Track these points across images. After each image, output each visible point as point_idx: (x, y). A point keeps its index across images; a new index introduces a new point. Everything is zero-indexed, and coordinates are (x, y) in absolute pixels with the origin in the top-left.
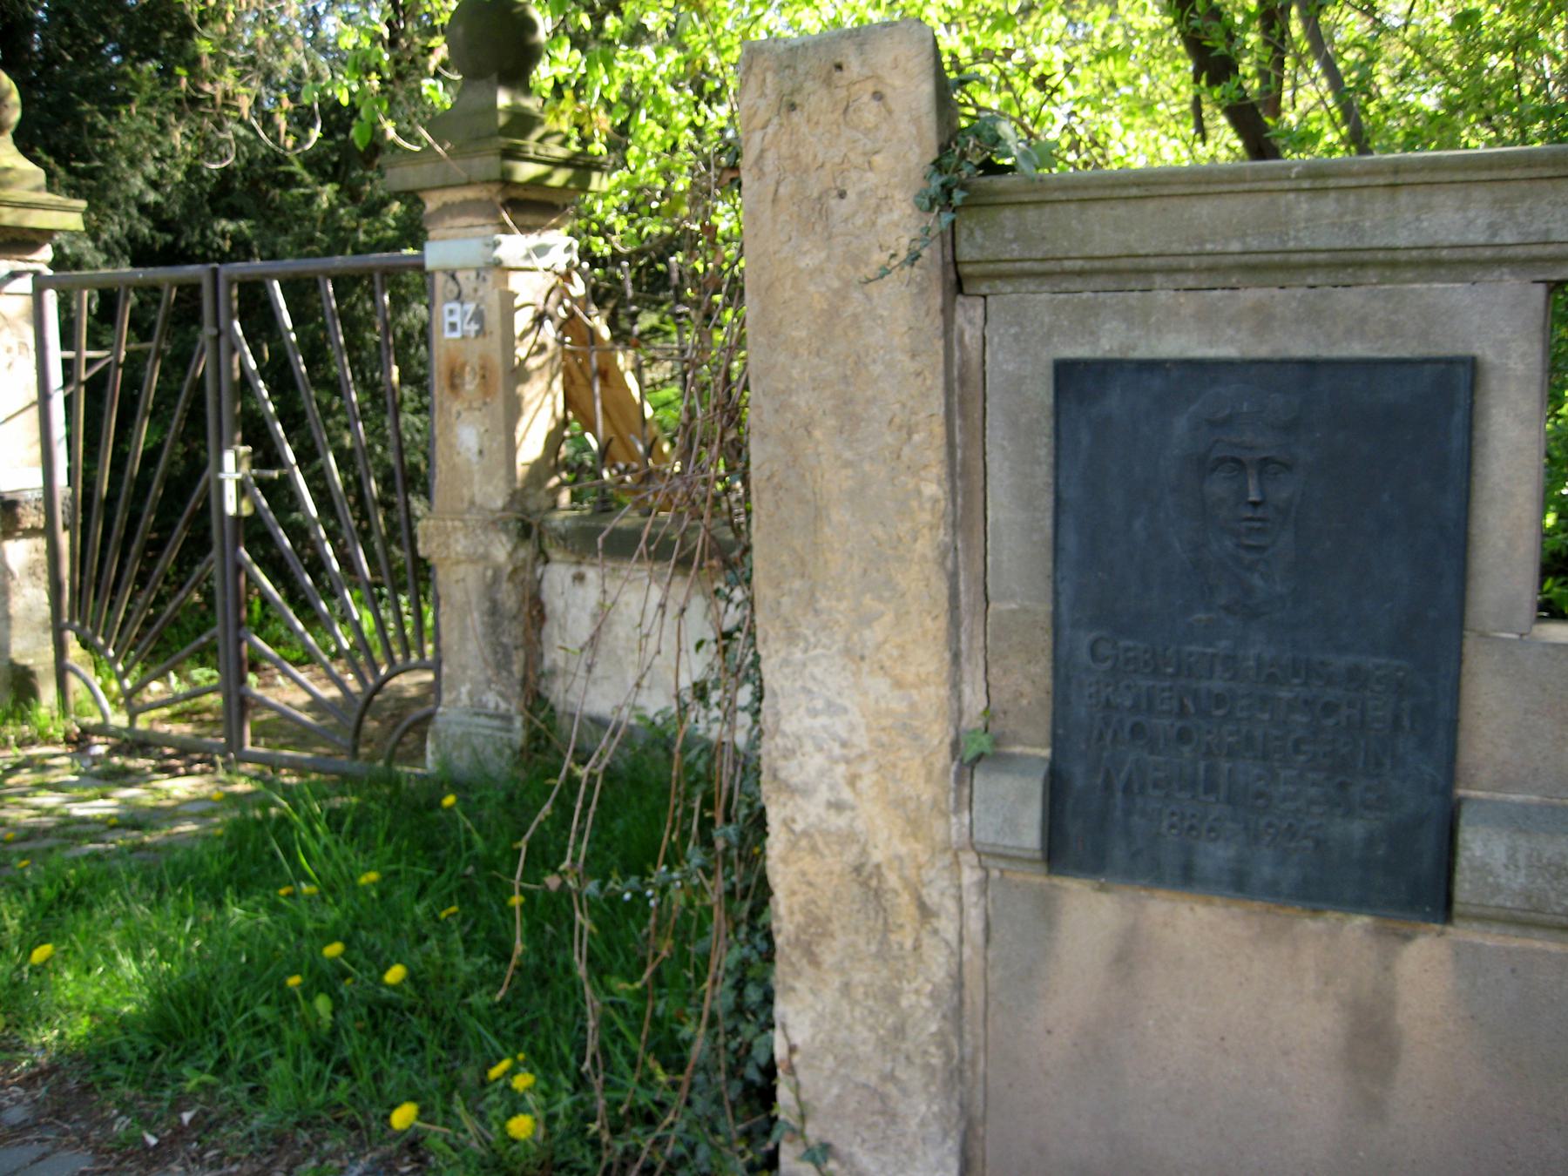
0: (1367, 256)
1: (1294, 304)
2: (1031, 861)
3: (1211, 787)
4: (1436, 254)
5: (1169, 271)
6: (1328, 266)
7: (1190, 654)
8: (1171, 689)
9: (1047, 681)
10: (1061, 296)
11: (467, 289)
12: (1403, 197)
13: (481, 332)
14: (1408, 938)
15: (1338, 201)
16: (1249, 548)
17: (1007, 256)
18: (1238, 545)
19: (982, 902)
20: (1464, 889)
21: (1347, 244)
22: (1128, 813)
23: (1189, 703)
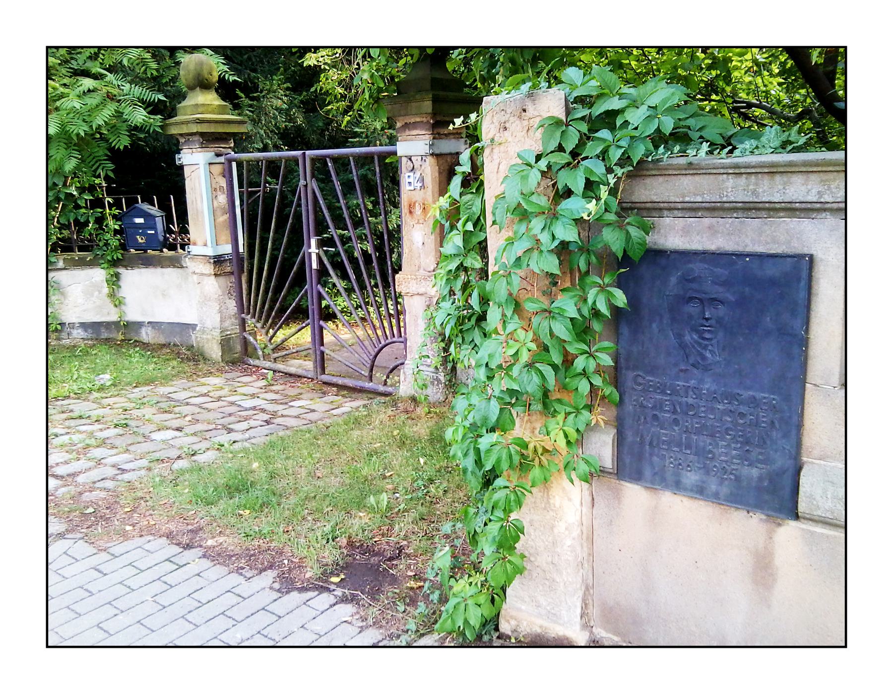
0: (761, 205)
1: (728, 226)
3: (688, 447)
4: (794, 206)
5: (670, 209)
11: (417, 165)
12: (778, 178)
13: (423, 187)
14: (779, 525)
15: (746, 179)
20: (802, 507)
21: (751, 200)
22: (651, 455)
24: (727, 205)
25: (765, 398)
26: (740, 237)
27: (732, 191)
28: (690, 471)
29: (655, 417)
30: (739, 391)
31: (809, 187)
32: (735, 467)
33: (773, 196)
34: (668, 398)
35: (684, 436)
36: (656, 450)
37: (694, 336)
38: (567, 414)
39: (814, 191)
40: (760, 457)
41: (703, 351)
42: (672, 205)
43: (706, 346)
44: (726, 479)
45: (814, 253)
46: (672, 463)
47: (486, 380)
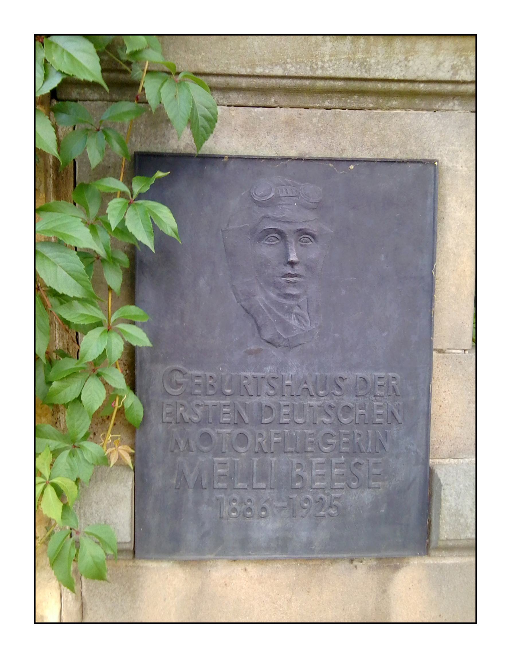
0: (370, 85)
1: (315, 120)
14: (397, 568)
15: (352, 42)
21: (359, 75)
22: (197, 504)
24: (320, 84)
26: (333, 138)
27: (331, 61)
28: (264, 517)
29: (206, 437)
30: (343, 374)
31: (441, 58)
32: (337, 495)
33: (391, 70)
34: (227, 401)
35: (255, 460)
36: (206, 493)
38: (56, 453)
39: (447, 65)
41: (286, 317)
42: (232, 81)
43: (291, 307)
44: (324, 516)
45: (439, 158)
46: (234, 510)
47: (101, 119)
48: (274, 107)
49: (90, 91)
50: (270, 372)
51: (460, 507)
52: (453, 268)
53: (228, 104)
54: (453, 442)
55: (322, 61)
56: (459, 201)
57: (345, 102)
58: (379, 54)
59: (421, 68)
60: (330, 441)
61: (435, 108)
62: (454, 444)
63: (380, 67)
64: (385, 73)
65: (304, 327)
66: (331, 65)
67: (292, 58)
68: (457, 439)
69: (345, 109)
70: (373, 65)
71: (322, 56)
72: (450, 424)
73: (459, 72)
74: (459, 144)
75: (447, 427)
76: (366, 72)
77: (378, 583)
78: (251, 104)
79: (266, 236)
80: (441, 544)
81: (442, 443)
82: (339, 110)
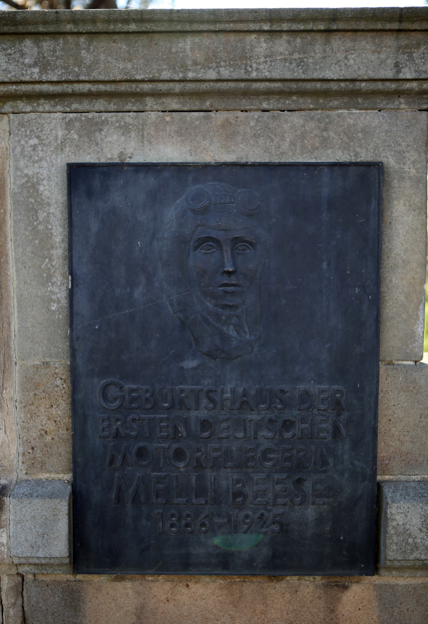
0: (309, 86)
1: (252, 123)
2: (61, 565)
6: (281, 93)
7: (182, 391)
8: (168, 419)
9: (67, 421)
10: (71, 115)
14: (345, 588)
15: (289, 42)
16: (225, 307)
17: (27, 78)
18: (216, 305)
19: (19, 602)
21: (296, 75)
23: (181, 429)
25: (323, 391)
27: (266, 62)
37: (208, 304)
40: (319, 487)
45: (384, 160)
48: (210, 111)
49: (23, 104)
50: (208, 385)
51: (408, 527)
52: (401, 275)
53: (162, 109)
54: (403, 458)
55: (256, 62)
56: (407, 204)
57: (283, 103)
58: (317, 53)
59: (361, 67)
60: (271, 456)
61: (379, 107)
62: (404, 460)
63: (318, 67)
64: (323, 74)
65: (242, 339)
66: (266, 67)
67: (225, 61)
68: (408, 455)
69: (284, 111)
70: (311, 65)
71: (257, 58)
72: (400, 439)
73: (402, 70)
74: (406, 144)
75: (397, 442)
76: (303, 73)
77: (325, 602)
78: (185, 109)
79: (202, 244)
80: (388, 563)
81: (392, 459)
82: (278, 112)
